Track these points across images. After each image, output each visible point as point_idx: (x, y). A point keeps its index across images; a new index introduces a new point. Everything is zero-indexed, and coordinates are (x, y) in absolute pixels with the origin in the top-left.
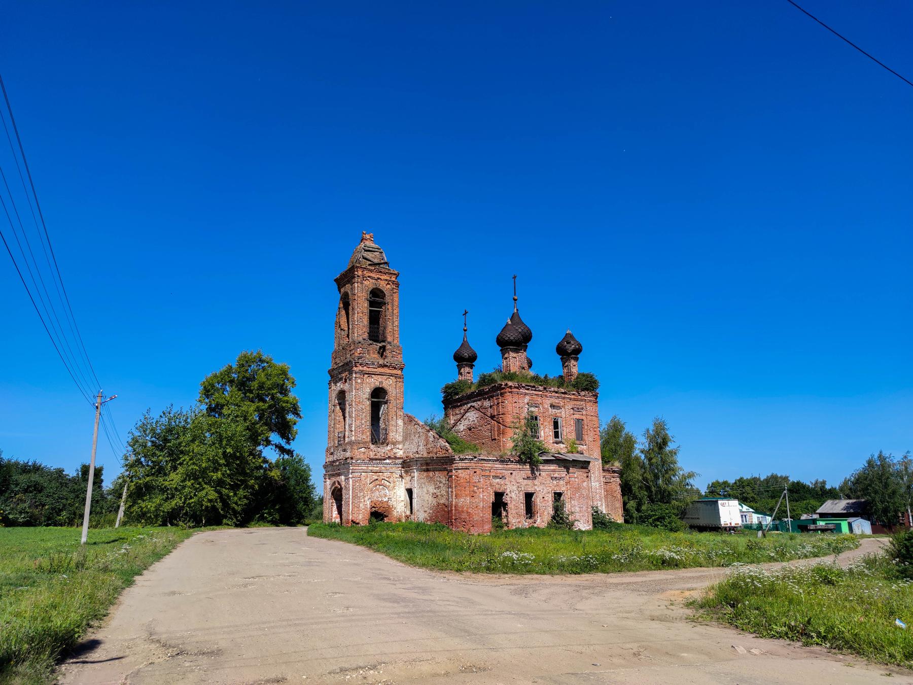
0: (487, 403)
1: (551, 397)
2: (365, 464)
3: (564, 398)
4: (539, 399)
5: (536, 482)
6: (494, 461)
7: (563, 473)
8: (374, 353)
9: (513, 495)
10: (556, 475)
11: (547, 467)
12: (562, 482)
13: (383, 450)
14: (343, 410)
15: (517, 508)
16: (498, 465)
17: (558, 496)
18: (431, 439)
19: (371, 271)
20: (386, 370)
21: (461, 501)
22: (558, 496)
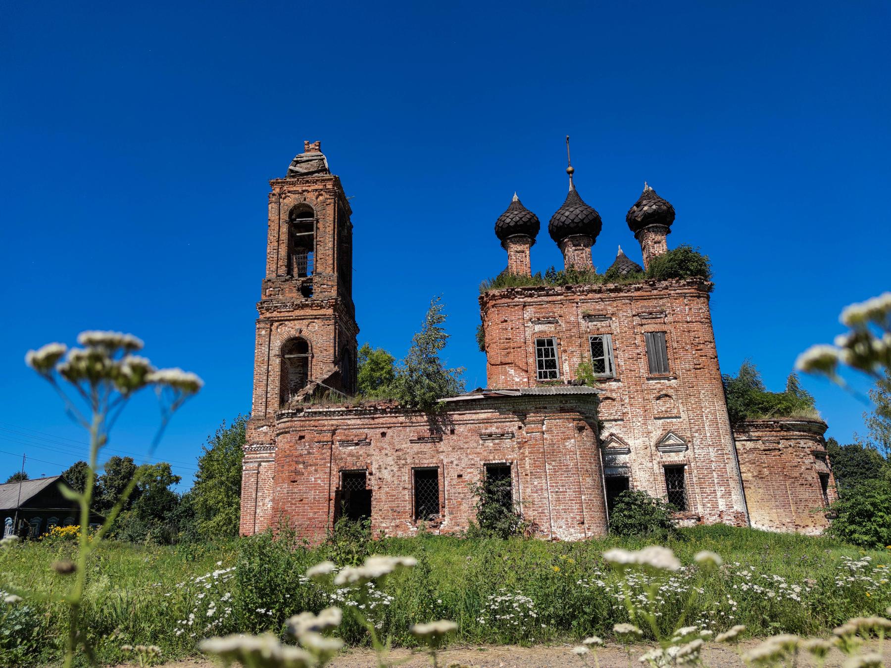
1: (584, 301)
2: (265, 449)
3: (615, 299)
5: (442, 446)
6: (341, 413)
7: (513, 426)
8: (291, 291)
9: (386, 474)
10: (493, 429)
11: (469, 416)
12: (507, 443)
15: (393, 498)
16: (353, 421)
17: (498, 473)
19: (293, 184)
20: (309, 312)
22: (498, 473)
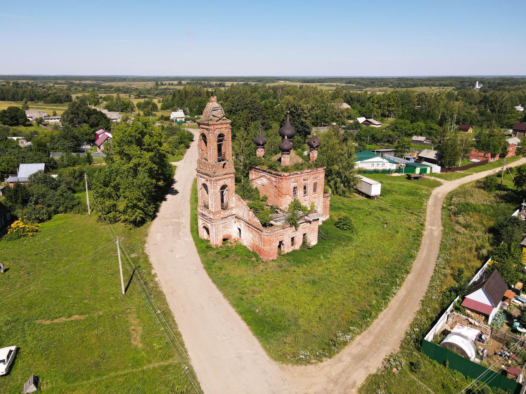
0: (273, 179)
4: (298, 178)
13: (227, 213)
14: (206, 143)
18: (251, 215)
20: (227, 176)
21: (265, 248)
